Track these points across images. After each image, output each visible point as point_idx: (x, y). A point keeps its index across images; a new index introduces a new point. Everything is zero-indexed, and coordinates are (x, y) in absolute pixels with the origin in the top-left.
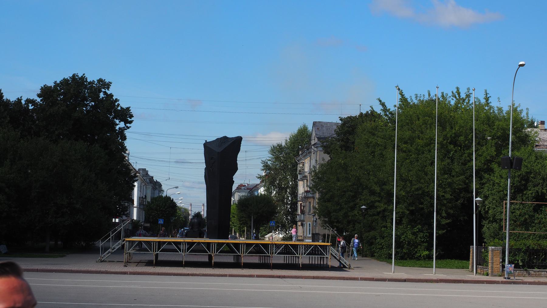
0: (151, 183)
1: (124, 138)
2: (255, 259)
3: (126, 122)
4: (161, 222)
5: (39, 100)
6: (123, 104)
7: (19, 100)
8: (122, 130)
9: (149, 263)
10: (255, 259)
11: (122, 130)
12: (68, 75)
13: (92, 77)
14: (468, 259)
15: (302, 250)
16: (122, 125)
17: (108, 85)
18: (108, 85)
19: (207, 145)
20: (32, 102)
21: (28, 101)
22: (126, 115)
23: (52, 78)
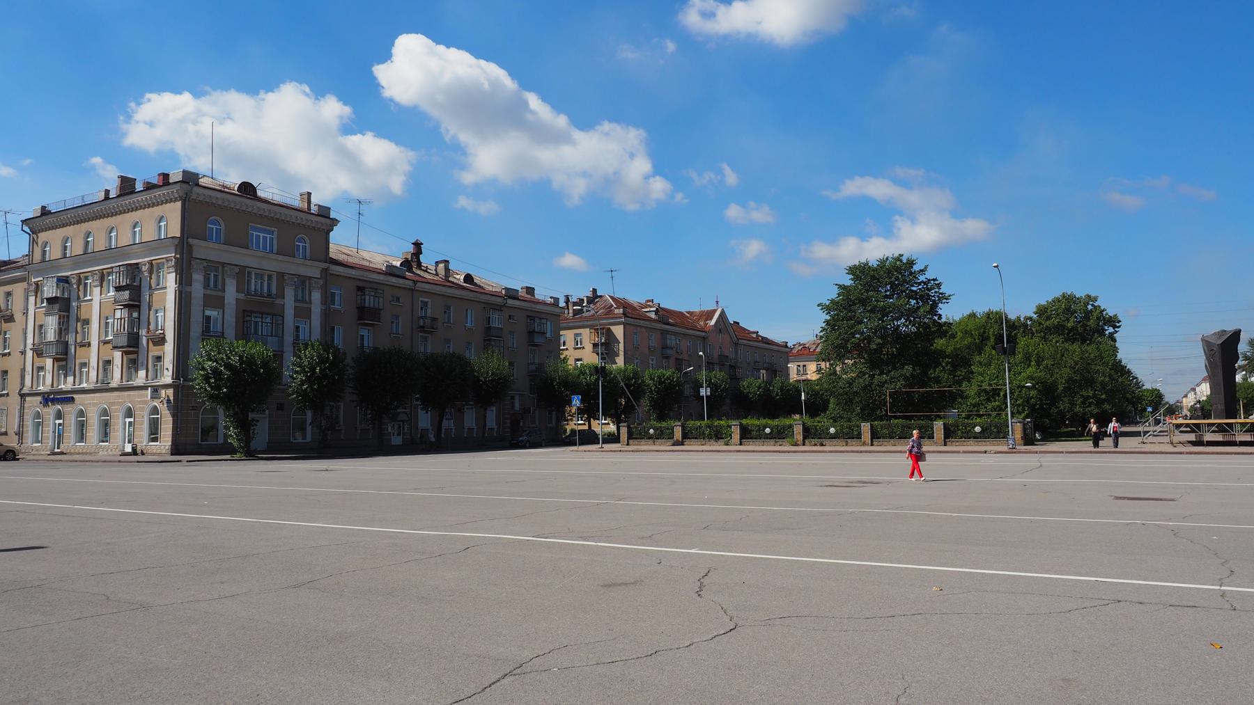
0: (775, 371)
1: (1115, 341)
2: (1218, 437)
3: (1115, 327)
4: (1150, 409)
5: (1035, 316)
6: (1110, 312)
7: (1019, 318)
8: (1111, 335)
9: (1194, 443)
10: (1218, 437)
11: (1111, 335)
12: (1058, 294)
13: (1080, 293)
14: (1025, 444)
15: (1238, 428)
16: (1111, 330)
17: (1095, 299)
18: (1095, 299)
19: (1206, 343)
20: (1031, 319)
21: (1027, 318)
22: (1113, 322)
23: (1045, 298)
